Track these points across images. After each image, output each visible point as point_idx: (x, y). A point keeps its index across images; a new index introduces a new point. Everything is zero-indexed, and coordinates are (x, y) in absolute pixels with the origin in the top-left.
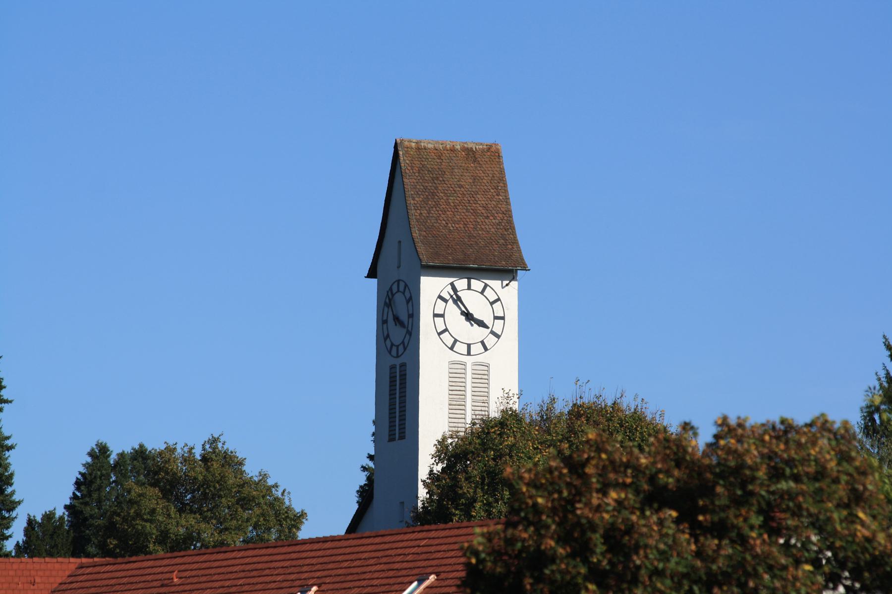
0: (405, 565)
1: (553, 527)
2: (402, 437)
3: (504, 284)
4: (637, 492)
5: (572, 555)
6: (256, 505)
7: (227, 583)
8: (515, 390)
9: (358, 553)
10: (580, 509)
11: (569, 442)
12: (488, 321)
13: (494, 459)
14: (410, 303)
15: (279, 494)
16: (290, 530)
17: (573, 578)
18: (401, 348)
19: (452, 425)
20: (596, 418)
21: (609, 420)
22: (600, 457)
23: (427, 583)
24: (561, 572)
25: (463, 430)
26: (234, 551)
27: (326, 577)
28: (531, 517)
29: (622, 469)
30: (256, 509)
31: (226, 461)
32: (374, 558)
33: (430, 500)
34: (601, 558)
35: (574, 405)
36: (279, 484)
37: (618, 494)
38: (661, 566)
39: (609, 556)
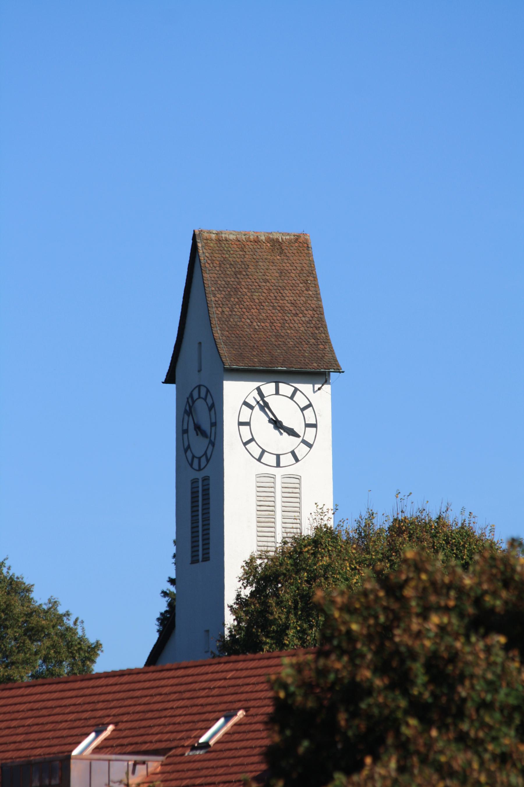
0: (210, 700)
1: (369, 656)
2: (206, 558)
3: (316, 388)
4: (461, 615)
5: (391, 687)
6: (46, 635)
7: (14, 724)
8: (330, 505)
9: (158, 687)
10: (399, 636)
11: (390, 561)
12: (299, 428)
13: (308, 582)
14: (213, 411)
15: (71, 623)
16: (83, 662)
17: (393, 712)
18: (203, 461)
19: (261, 544)
20: (420, 534)
21: (434, 536)
22: (419, 579)
23: (235, 720)
24: (379, 705)
25: (274, 549)
26: (20, 688)
27: (123, 714)
28: (344, 645)
29: (444, 591)
30: (45, 640)
31: (12, 588)
32: (175, 693)
33: (238, 628)
34: (422, 690)
35: (395, 520)
36: (71, 611)
37: (441, 618)
38: (489, 697)
39: (431, 687)
